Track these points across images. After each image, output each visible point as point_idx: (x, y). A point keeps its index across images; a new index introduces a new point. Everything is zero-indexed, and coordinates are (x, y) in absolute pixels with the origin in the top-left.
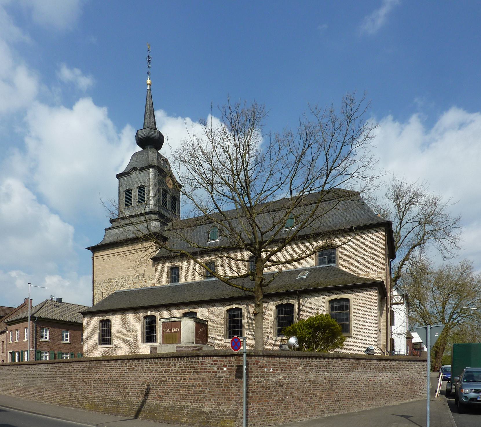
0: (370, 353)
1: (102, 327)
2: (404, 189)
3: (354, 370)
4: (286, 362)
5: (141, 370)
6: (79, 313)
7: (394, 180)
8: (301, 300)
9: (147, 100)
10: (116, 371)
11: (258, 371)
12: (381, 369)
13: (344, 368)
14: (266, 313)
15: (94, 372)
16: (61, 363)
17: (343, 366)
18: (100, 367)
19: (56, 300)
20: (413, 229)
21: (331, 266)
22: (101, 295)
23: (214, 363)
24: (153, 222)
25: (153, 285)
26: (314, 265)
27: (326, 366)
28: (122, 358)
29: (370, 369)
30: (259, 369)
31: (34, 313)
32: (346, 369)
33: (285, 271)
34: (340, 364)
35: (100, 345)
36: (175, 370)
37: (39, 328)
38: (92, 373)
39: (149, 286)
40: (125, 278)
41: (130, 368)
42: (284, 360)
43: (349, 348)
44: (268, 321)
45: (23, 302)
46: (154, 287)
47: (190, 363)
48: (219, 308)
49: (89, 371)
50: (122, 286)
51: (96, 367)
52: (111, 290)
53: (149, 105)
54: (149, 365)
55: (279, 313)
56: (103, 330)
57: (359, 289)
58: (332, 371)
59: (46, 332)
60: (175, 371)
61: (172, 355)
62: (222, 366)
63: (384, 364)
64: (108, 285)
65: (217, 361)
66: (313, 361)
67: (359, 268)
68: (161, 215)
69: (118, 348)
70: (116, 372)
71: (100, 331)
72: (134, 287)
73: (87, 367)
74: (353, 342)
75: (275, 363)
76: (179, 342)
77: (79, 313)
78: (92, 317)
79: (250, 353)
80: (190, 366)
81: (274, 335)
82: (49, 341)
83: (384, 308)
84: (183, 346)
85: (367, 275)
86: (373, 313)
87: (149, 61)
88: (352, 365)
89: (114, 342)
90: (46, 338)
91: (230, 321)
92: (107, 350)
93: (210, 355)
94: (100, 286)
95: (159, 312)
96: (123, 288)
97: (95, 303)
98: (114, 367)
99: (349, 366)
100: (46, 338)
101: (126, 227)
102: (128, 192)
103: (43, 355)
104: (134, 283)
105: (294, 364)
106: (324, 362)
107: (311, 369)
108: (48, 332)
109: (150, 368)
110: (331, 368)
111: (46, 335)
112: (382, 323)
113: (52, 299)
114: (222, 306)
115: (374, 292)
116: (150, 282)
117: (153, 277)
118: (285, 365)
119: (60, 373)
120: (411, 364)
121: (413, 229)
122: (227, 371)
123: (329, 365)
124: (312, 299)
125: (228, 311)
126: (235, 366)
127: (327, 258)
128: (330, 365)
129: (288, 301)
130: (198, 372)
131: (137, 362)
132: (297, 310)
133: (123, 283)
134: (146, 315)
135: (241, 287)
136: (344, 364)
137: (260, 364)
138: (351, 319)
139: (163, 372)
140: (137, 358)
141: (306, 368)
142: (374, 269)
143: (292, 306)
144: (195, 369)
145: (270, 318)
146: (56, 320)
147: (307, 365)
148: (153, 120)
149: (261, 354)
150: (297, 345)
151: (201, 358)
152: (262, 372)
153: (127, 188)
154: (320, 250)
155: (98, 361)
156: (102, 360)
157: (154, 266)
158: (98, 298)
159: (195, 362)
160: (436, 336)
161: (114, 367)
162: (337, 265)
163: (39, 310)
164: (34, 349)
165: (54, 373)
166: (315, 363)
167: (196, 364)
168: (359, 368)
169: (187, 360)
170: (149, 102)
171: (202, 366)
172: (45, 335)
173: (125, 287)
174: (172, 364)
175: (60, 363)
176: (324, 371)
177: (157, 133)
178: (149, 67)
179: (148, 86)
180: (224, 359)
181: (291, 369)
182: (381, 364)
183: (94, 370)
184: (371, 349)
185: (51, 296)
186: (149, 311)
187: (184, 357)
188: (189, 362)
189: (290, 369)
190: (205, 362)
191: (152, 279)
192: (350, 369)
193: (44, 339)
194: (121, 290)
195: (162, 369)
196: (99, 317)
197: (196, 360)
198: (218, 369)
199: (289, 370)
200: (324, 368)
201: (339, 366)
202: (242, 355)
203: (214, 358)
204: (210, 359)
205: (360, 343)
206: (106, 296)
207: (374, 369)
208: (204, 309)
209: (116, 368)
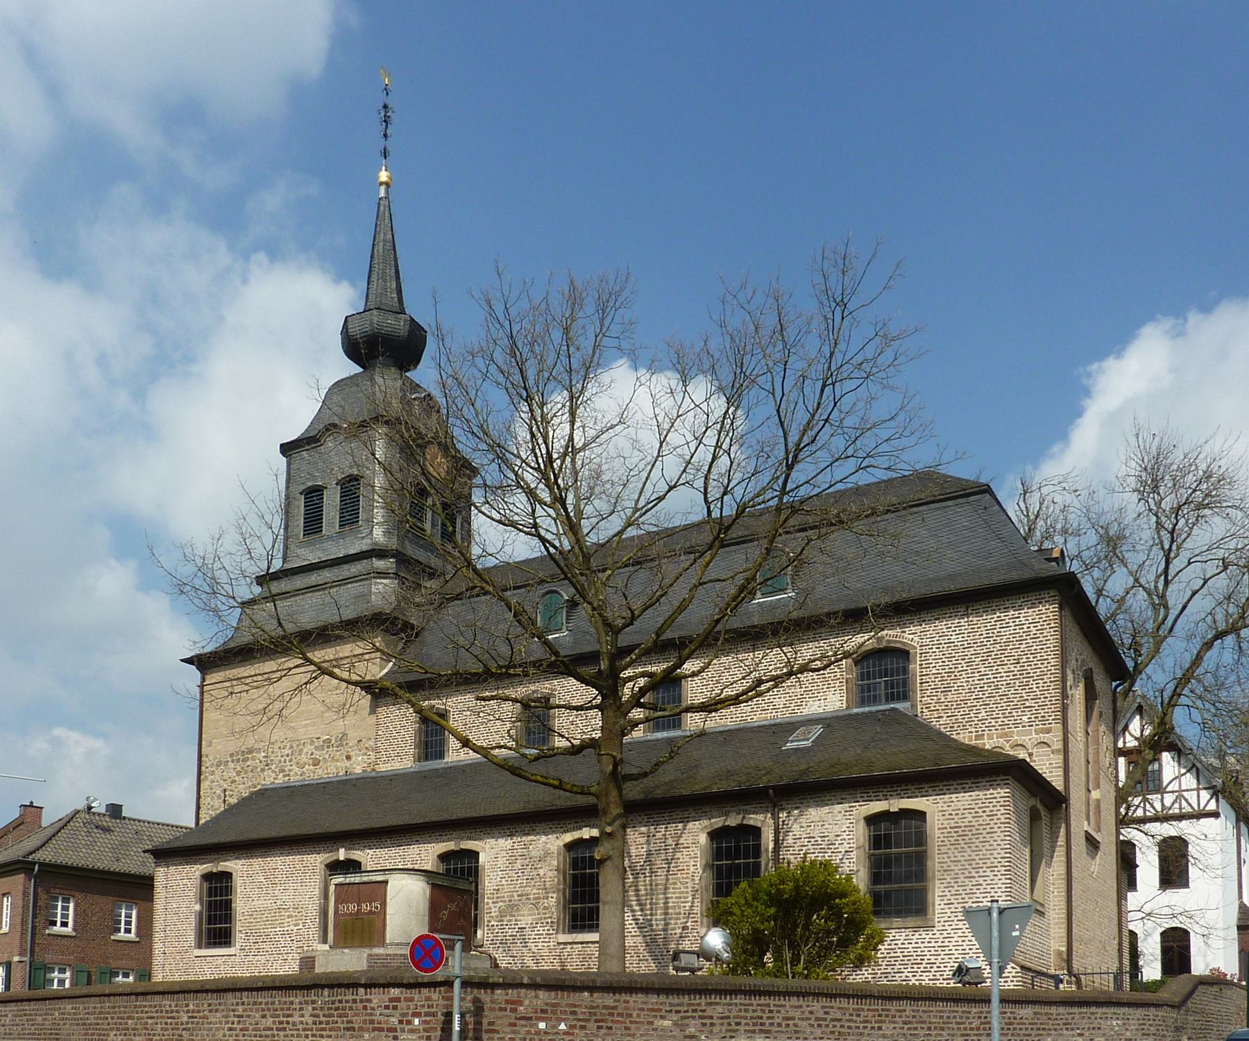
0: (967, 978)
1: (210, 895)
2: (1177, 458)
3: (866, 1032)
4: (616, 1004)
5: (220, 1023)
6: (144, 852)
7: (1137, 436)
8: (783, 815)
9: (378, 229)
10: (164, 1026)
11: (514, 1028)
12: (971, 1029)
13: (827, 1026)
14: (678, 855)
15: (111, 1026)
16: (36, 1000)
17: (825, 1019)
18: (125, 1012)
19: (103, 811)
20: (1204, 585)
21: (893, 709)
22: (219, 797)
23: (391, 1004)
24: (379, 581)
25: (369, 769)
26: (844, 706)
27: (761, 1018)
28: (178, 988)
29: (929, 1029)
30: (518, 1022)
31: (32, 849)
32: (834, 1026)
33: (757, 724)
34: (811, 1012)
35: (200, 947)
36: (301, 1023)
37: (43, 896)
38: (106, 1030)
39: (358, 770)
40: (291, 747)
41: (196, 1017)
42: (608, 999)
43: (924, 962)
44: (687, 878)
45: (15, 813)
46: (373, 774)
47: (337, 1005)
48: (544, 838)
49: (98, 1024)
50: (282, 771)
51: (115, 1013)
52: (250, 784)
53: (381, 244)
54: (240, 1008)
55: (717, 854)
56: (210, 902)
57: (955, 783)
58: (782, 1032)
59: (65, 908)
60: (301, 1027)
61: (295, 981)
62: (410, 1012)
63: (983, 1015)
64: (242, 768)
65: (398, 1000)
66: (711, 1004)
67: (980, 716)
68: (402, 559)
69: (251, 958)
70: (162, 1029)
71: (202, 905)
72: (314, 772)
73: (95, 1013)
74: (937, 945)
75: (575, 1006)
76: (382, 942)
77: (144, 852)
78: (181, 864)
79: (488, 977)
80: (335, 1013)
81: (702, 923)
82: (74, 934)
83: (1058, 837)
84: (387, 955)
85: (1006, 735)
86: (996, 856)
87: (386, 121)
88: (858, 1016)
89: (239, 938)
90: (64, 924)
91: (574, 877)
92: (219, 962)
93: (381, 981)
94: (218, 772)
95: (371, 852)
96: (284, 776)
97: (202, 822)
98: (159, 1014)
99: (848, 1017)
100: (64, 924)
101: (301, 597)
102: (314, 495)
103: (53, 975)
104: (316, 763)
105: (643, 1009)
106: (752, 1005)
107: (704, 1025)
108: (71, 905)
109: (242, 1017)
110: (779, 1025)
111: (65, 916)
112: (1053, 884)
113: (90, 808)
114: (553, 832)
115: (999, 790)
116: (360, 758)
117: (371, 743)
118: (612, 1015)
119: (33, 1028)
120: (1093, 1013)
121: (1204, 585)
122: (421, 1028)
123: (771, 1015)
124: (814, 813)
125: (570, 847)
126: (439, 1013)
127: (883, 684)
128: (775, 1014)
129: (744, 818)
130: (353, 1029)
131: (212, 999)
132: (771, 846)
133: (285, 762)
134: (335, 858)
135: (556, 783)
136: (826, 1013)
137: (522, 1008)
138: (930, 874)
139: (272, 1029)
140: (214, 988)
141: (686, 1021)
142: (1025, 718)
143: (756, 832)
144: (348, 1022)
145: (692, 869)
146: (98, 871)
147: (690, 1014)
148: (394, 286)
149: (525, 981)
150: (726, 955)
151: (362, 990)
152: (529, 1032)
153: (310, 484)
154: (864, 659)
155: (120, 995)
156: (131, 994)
157: (373, 711)
158: (212, 806)
159: (347, 1002)
160: (1014, 934)
161: (159, 1014)
162: (914, 706)
163: (47, 842)
164: (26, 959)
165: (20, 1028)
166: (719, 1009)
167: (351, 1008)
168: (884, 1026)
169: (329, 996)
170: (382, 235)
171: (365, 1012)
172: (63, 916)
173: (289, 775)
174: (294, 1006)
175: (33, 1000)
176: (754, 1032)
177: (402, 323)
178: (385, 136)
179: (383, 189)
180: (414, 994)
181: (633, 1026)
182: (970, 1012)
183: (110, 1020)
184: (970, 966)
185: (88, 798)
186: (343, 847)
187: (323, 987)
188: (333, 1003)
189: (628, 1025)
190: (370, 1001)
191: (367, 748)
192: (849, 1027)
193: (58, 929)
194: (277, 781)
195: (271, 1020)
196: (202, 864)
197: (350, 997)
198: (401, 1022)
199: (626, 1028)
200: (754, 1024)
201: (808, 1019)
202: (448, 984)
203: (393, 990)
204: (384, 994)
205: (960, 948)
206: (233, 801)
207: (942, 1029)
208: (501, 841)
209: (163, 1017)
